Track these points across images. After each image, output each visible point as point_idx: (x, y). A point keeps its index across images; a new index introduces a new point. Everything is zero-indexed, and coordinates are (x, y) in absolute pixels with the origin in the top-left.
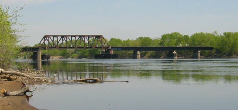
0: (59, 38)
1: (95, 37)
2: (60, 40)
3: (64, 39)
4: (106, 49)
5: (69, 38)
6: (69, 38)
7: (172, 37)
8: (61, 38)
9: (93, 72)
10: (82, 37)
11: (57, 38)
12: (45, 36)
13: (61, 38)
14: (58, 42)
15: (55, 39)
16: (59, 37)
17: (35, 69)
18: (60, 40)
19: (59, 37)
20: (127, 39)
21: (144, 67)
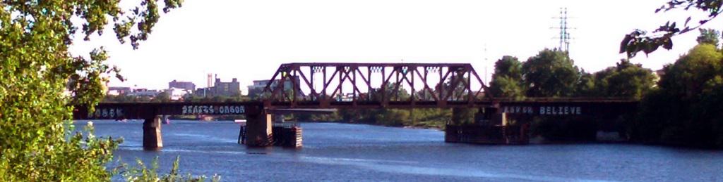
0: (389, 70)
1: (445, 70)
2: (330, 81)
3: (344, 75)
4: (716, 8)
5: (359, 72)
6: (359, 72)
7: (36, 11)
8: (393, 73)
9: (178, 151)
10: (347, 69)
11: (324, 71)
12: (286, 65)
13: (393, 73)
14: (326, 85)
15: (372, 74)
16: (328, 69)
17: (142, 162)
18: (330, 81)
19: (328, 69)
20: (267, 72)
21: (215, 139)
